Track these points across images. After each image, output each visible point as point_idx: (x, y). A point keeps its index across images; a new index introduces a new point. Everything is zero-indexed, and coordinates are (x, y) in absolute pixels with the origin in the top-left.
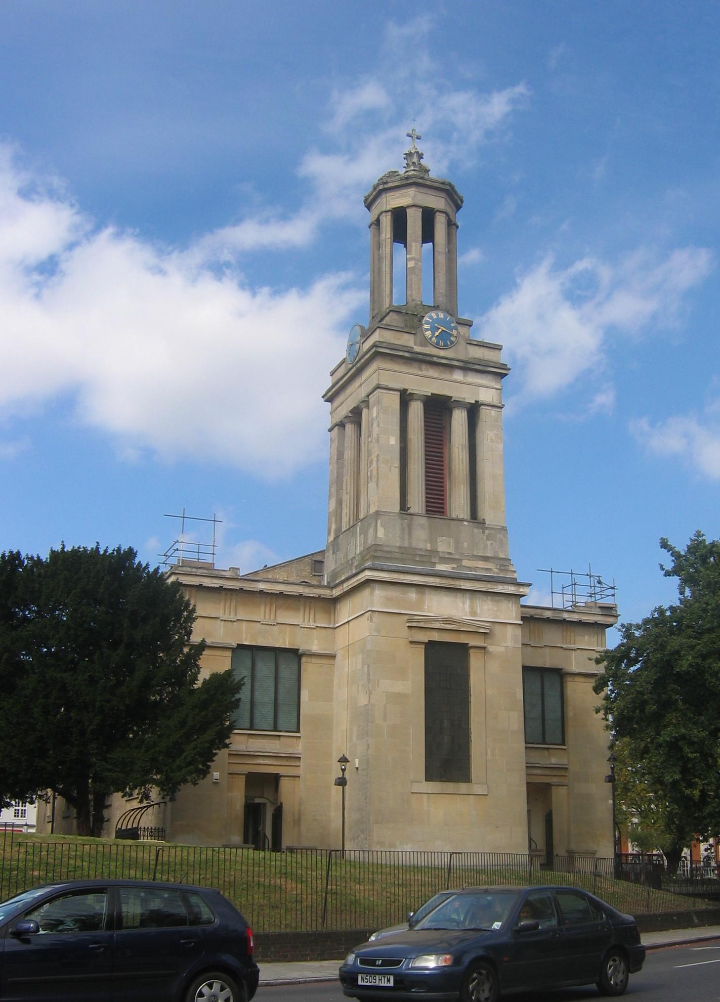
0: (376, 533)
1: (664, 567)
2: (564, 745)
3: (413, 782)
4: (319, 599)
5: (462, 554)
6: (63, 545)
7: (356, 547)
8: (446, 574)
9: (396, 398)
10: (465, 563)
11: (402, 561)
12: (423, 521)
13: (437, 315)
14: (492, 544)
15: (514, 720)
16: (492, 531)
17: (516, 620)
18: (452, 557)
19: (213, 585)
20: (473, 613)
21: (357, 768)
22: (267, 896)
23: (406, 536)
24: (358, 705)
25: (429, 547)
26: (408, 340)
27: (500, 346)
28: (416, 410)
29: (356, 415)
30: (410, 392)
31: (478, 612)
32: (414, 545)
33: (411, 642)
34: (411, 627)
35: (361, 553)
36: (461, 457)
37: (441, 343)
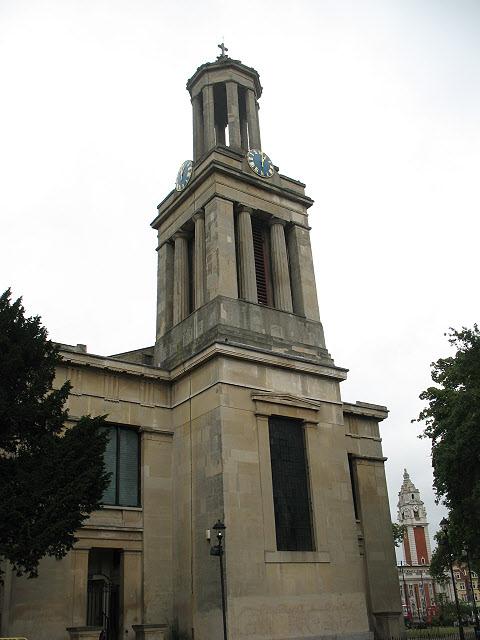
0: (220, 314)
2: (139, 505)
4: (157, 381)
10: (294, 348)
12: (257, 309)
20: (305, 392)
21: (209, 540)
24: (207, 476)
26: (239, 166)
28: (246, 219)
29: (188, 232)
35: (201, 337)
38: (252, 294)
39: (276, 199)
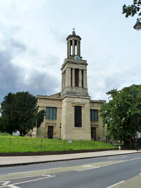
4: (59, 100)
7: (65, 92)
9: (70, 69)
10: (81, 94)
11: (73, 94)
15: (89, 118)
22: (127, 132)
25: (75, 91)
26: (72, 60)
28: (74, 71)
29: (65, 72)
32: (73, 91)
38: (74, 85)
39: (80, 65)
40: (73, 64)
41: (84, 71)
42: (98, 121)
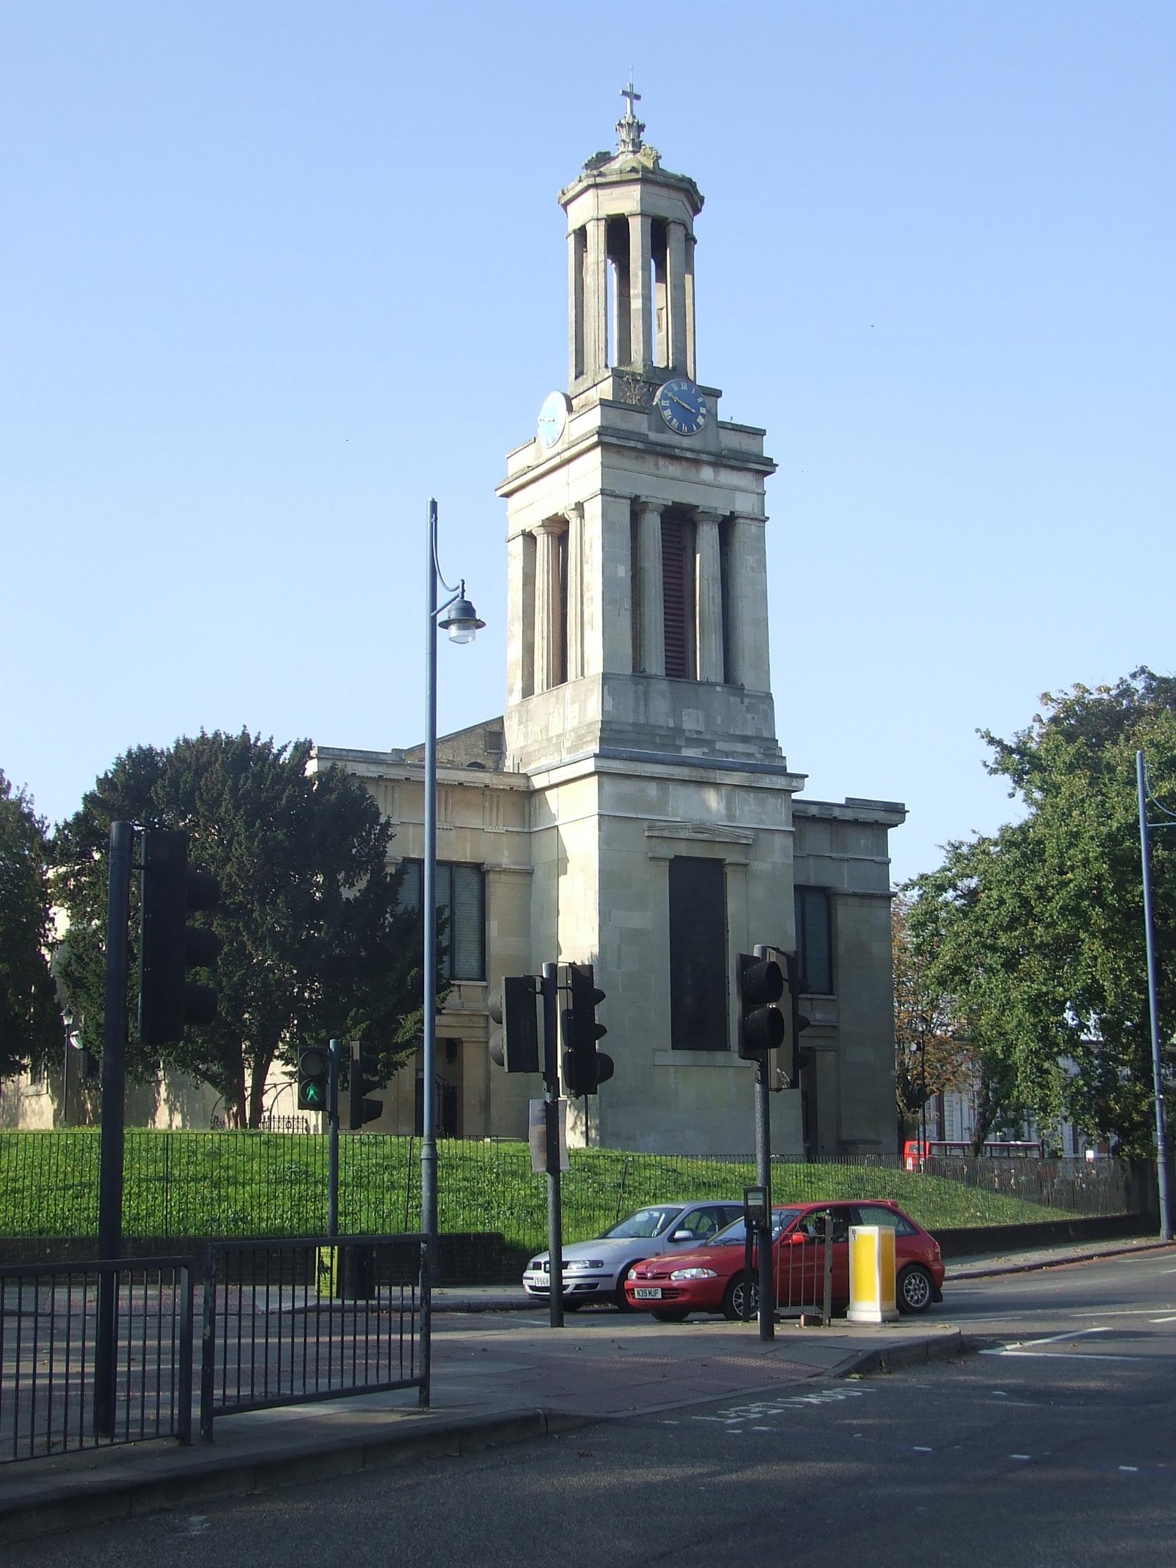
1: (987, 764)
3: (655, 1050)
5: (716, 733)
6: (203, 732)
8: (690, 761)
10: (719, 745)
11: (637, 744)
12: (663, 686)
13: (680, 387)
14: (753, 718)
16: (752, 700)
17: (786, 825)
18: (702, 737)
19: (370, 775)
23: (642, 708)
25: (671, 724)
27: (761, 430)
28: (652, 524)
30: (644, 500)
31: (738, 814)
32: (652, 721)
33: (651, 859)
34: (652, 837)
36: (711, 594)
37: (684, 428)
38: (655, 663)
40: (649, 464)
41: (744, 530)
42: (831, 992)
